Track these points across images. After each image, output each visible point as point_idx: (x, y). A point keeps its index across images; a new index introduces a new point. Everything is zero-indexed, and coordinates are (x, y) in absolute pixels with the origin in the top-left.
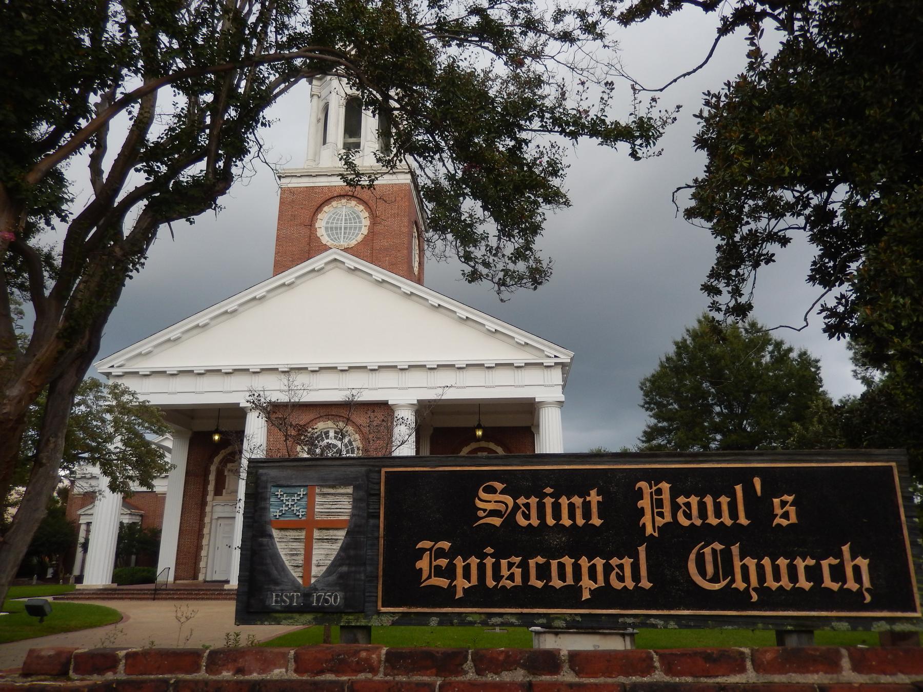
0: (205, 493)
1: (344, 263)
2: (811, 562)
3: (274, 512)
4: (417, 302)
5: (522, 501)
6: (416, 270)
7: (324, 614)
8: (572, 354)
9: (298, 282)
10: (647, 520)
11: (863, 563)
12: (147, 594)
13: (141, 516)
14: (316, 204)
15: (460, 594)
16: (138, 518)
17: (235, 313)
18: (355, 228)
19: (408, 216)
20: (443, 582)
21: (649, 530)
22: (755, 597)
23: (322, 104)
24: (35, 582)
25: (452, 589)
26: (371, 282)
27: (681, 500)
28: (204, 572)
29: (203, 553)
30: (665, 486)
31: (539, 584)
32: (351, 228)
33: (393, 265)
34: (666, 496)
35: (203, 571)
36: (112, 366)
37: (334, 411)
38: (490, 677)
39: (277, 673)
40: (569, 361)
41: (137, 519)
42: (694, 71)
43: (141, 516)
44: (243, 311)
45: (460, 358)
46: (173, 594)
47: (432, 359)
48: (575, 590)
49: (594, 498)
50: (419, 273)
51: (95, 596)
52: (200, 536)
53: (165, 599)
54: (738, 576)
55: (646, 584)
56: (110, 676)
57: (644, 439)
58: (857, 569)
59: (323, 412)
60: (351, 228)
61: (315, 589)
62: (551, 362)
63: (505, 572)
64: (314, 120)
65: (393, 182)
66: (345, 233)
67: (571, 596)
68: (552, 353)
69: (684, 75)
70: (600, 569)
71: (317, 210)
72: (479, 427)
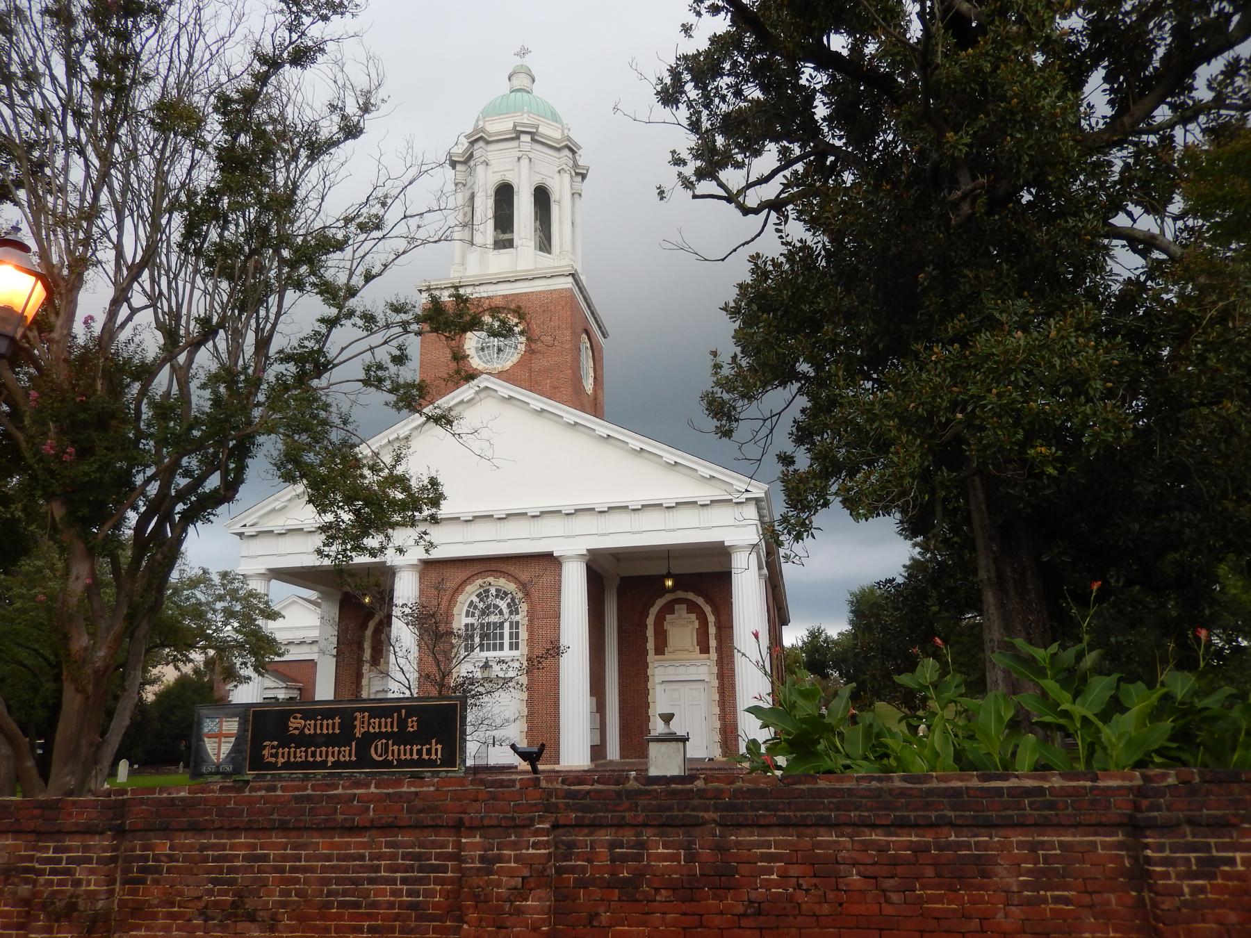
0: (360, 662)
2: (419, 747)
3: (206, 730)
5: (308, 722)
6: (589, 385)
7: (226, 775)
8: (766, 487)
10: (357, 730)
11: (439, 747)
13: (300, 689)
15: (279, 765)
16: (295, 691)
20: (273, 760)
21: (358, 735)
22: (395, 762)
23: (468, 194)
24: (181, 770)
25: (276, 762)
27: (372, 720)
30: (367, 714)
31: (311, 759)
34: (366, 719)
36: (245, 526)
37: (494, 566)
38: (253, 794)
39: (182, 794)
40: (763, 495)
41: (295, 694)
42: (753, 240)
43: (300, 689)
45: (635, 497)
47: (601, 500)
48: (325, 762)
49: (337, 720)
50: (595, 390)
54: (390, 754)
55: (353, 758)
56: (125, 797)
58: (436, 750)
59: (477, 568)
61: (221, 764)
62: (742, 499)
63: (298, 755)
67: (323, 765)
69: (743, 245)
70: (336, 753)
72: (669, 576)
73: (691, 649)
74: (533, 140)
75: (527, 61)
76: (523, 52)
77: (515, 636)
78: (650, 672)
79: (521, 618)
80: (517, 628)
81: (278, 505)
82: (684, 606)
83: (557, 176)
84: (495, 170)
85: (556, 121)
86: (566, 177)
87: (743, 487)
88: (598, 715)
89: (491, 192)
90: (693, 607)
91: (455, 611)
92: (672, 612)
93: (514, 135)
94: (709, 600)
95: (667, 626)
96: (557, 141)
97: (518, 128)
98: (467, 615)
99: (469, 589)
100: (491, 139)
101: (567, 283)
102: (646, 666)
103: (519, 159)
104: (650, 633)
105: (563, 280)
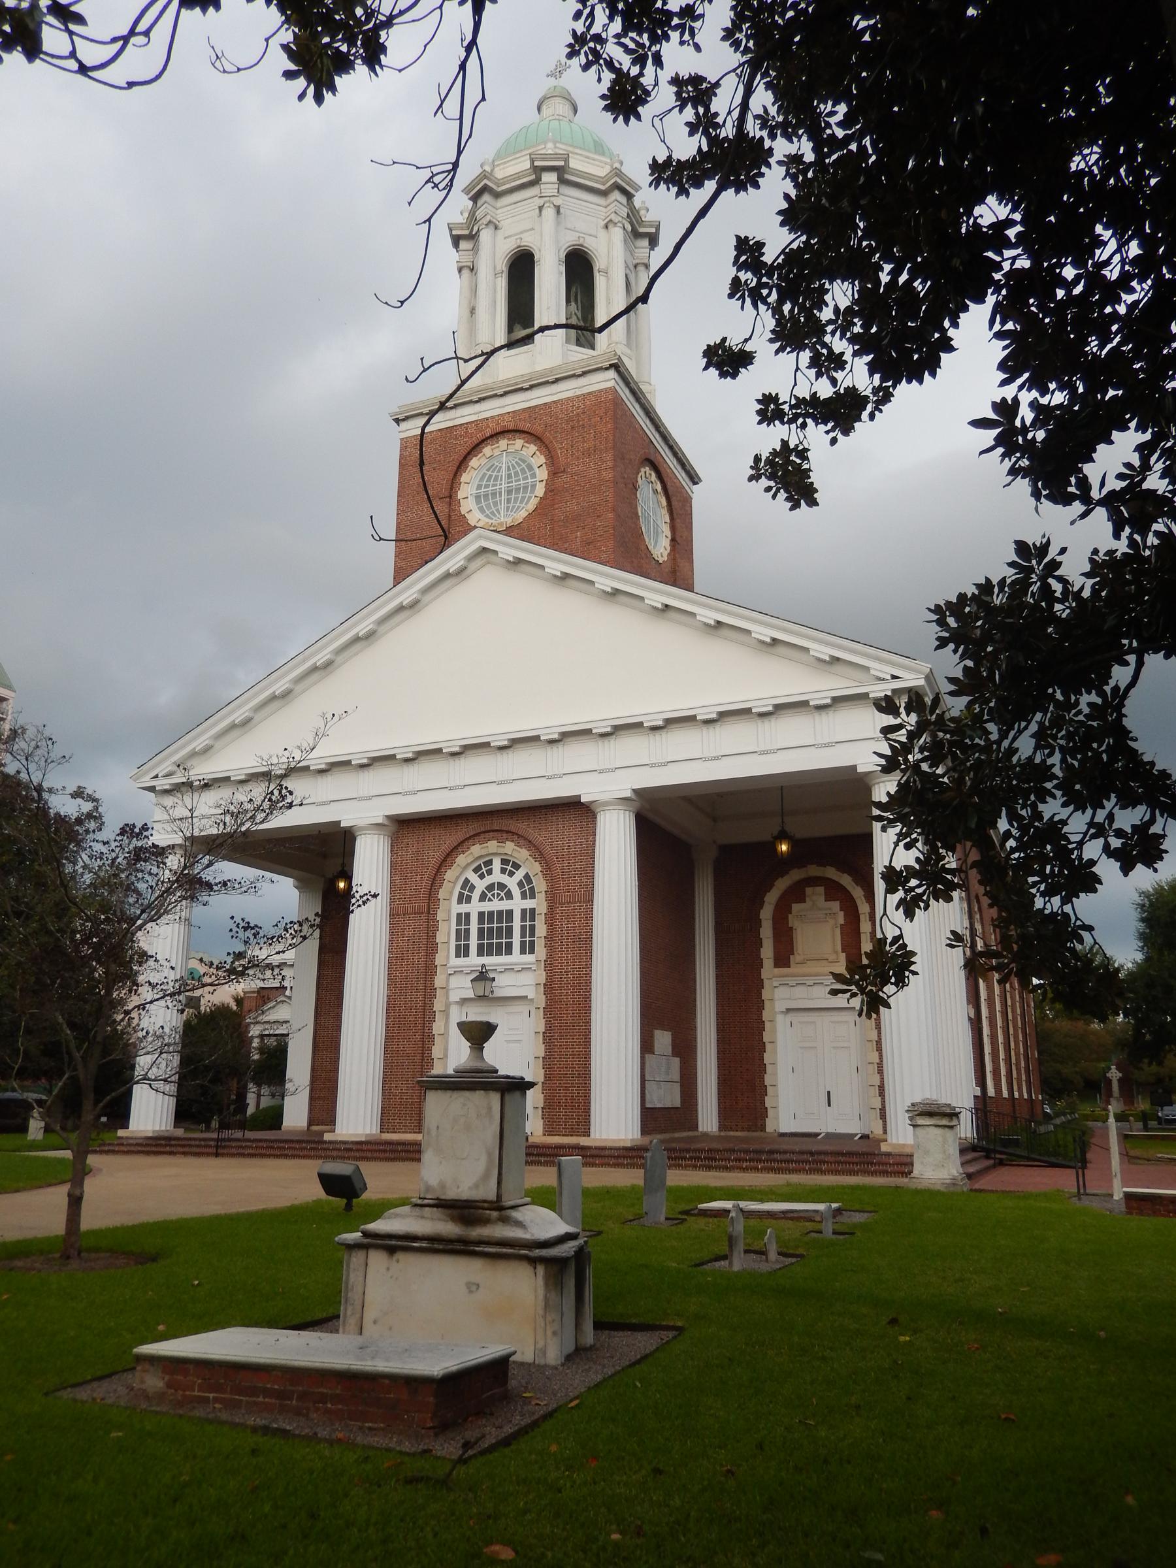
4: (626, 605)
14: (456, 457)
17: (330, 669)
18: (525, 488)
19: (614, 447)
26: (546, 580)
32: (518, 490)
33: (589, 544)
36: (156, 776)
40: (922, 682)
44: (344, 663)
45: (706, 702)
65: (585, 390)
66: (509, 501)
68: (887, 671)
71: (459, 467)
72: (783, 836)
73: (832, 957)
74: (562, 181)
78: (765, 994)
79: (539, 904)
80: (533, 919)
82: (821, 890)
83: (602, 233)
84: (508, 233)
85: (603, 154)
86: (617, 234)
87: (887, 671)
88: (677, 1060)
89: (502, 265)
90: (835, 891)
91: (442, 894)
92: (802, 899)
93: (533, 177)
94: (843, 867)
95: (793, 921)
97: (536, 164)
98: (460, 901)
99: (462, 860)
100: (500, 189)
101: (608, 380)
102: (760, 984)
103: (541, 208)
104: (766, 932)
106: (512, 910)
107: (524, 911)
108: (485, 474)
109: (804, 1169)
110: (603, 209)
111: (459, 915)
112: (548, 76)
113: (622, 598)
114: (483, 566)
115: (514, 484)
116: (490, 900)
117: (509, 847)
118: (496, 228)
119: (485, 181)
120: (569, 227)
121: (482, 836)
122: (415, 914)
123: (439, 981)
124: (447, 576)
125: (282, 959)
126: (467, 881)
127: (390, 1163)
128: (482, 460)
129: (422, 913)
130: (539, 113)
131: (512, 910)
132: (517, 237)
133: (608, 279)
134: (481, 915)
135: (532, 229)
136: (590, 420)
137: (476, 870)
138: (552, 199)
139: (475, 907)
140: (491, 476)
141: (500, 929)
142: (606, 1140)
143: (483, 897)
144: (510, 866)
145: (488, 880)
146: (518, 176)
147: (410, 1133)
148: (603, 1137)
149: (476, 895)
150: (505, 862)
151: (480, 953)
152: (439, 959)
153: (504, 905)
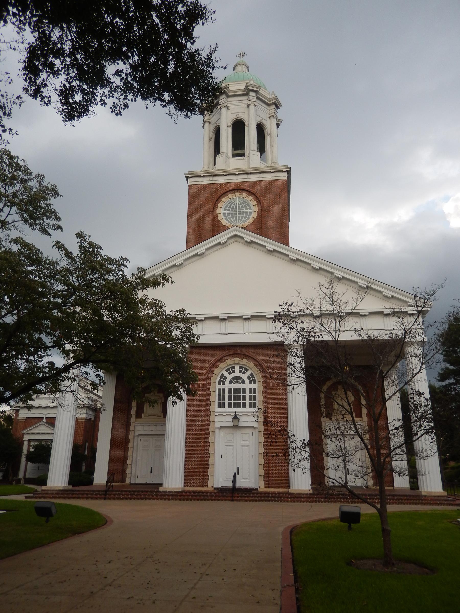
0: (129, 417)
1: (242, 238)
9: (207, 252)
12: (99, 494)
18: (247, 213)
23: (213, 128)
28: (129, 476)
29: (129, 462)
32: (243, 213)
35: (128, 476)
37: (239, 351)
46: (119, 494)
51: (58, 496)
52: (126, 449)
53: (114, 499)
57: (439, 378)
60: (243, 213)
64: (207, 139)
65: (274, 178)
66: (239, 217)
71: (217, 200)
75: (245, 59)
76: (242, 55)
77: (253, 398)
79: (259, 386)
81: (222, 240)
83: (268, 119)
89: (230, 124)
93: (245, 92)
96: (270, 99)
97: (249, 87)
98: (220, 383)
99: (222, 365)
100: (230, 94)
103: (248, 105)
105: (281, 174)
106: (245, 389)
107: (251, 389)
108: (227, 205)
109: (396, 503)
110: (268, 111)
111: (219, 390)
112: (237, 56)
113: (299, 263)
114: (234, 242)
115: (234, 211)
116: (234, 384)
117: (245, 361)
118: (228, 109)
119: (225, 90)
120: (258, 114)
121: (231, 356)
122: (200, 388)
123: (211, 419)
124: (219, 244)
125: (39, 405)
126: (223, 375)
127: (200, 502)
128: (227, 199)
129: (203, 388)
130: (234, 71)
131: (245, 389)
132: (237, 114)
133: (271, 138)
134: (230, 390)
135: (244, 112)
136: (277, 190)
137: (227, 370)
138: (254, 102)
139: (227, 386)
140: (230, 206)
141: (239, 397)
142: (301, 490)
143: (231, 382)
144: (243, 370)
145: (233, 375)
146: (239, 91)
147: (199, 487)
148: (173, 487)
149: (227, 381)
150: (240, 367)
151: (230, 406)
152: (211, 409)
153: (241, 386)
